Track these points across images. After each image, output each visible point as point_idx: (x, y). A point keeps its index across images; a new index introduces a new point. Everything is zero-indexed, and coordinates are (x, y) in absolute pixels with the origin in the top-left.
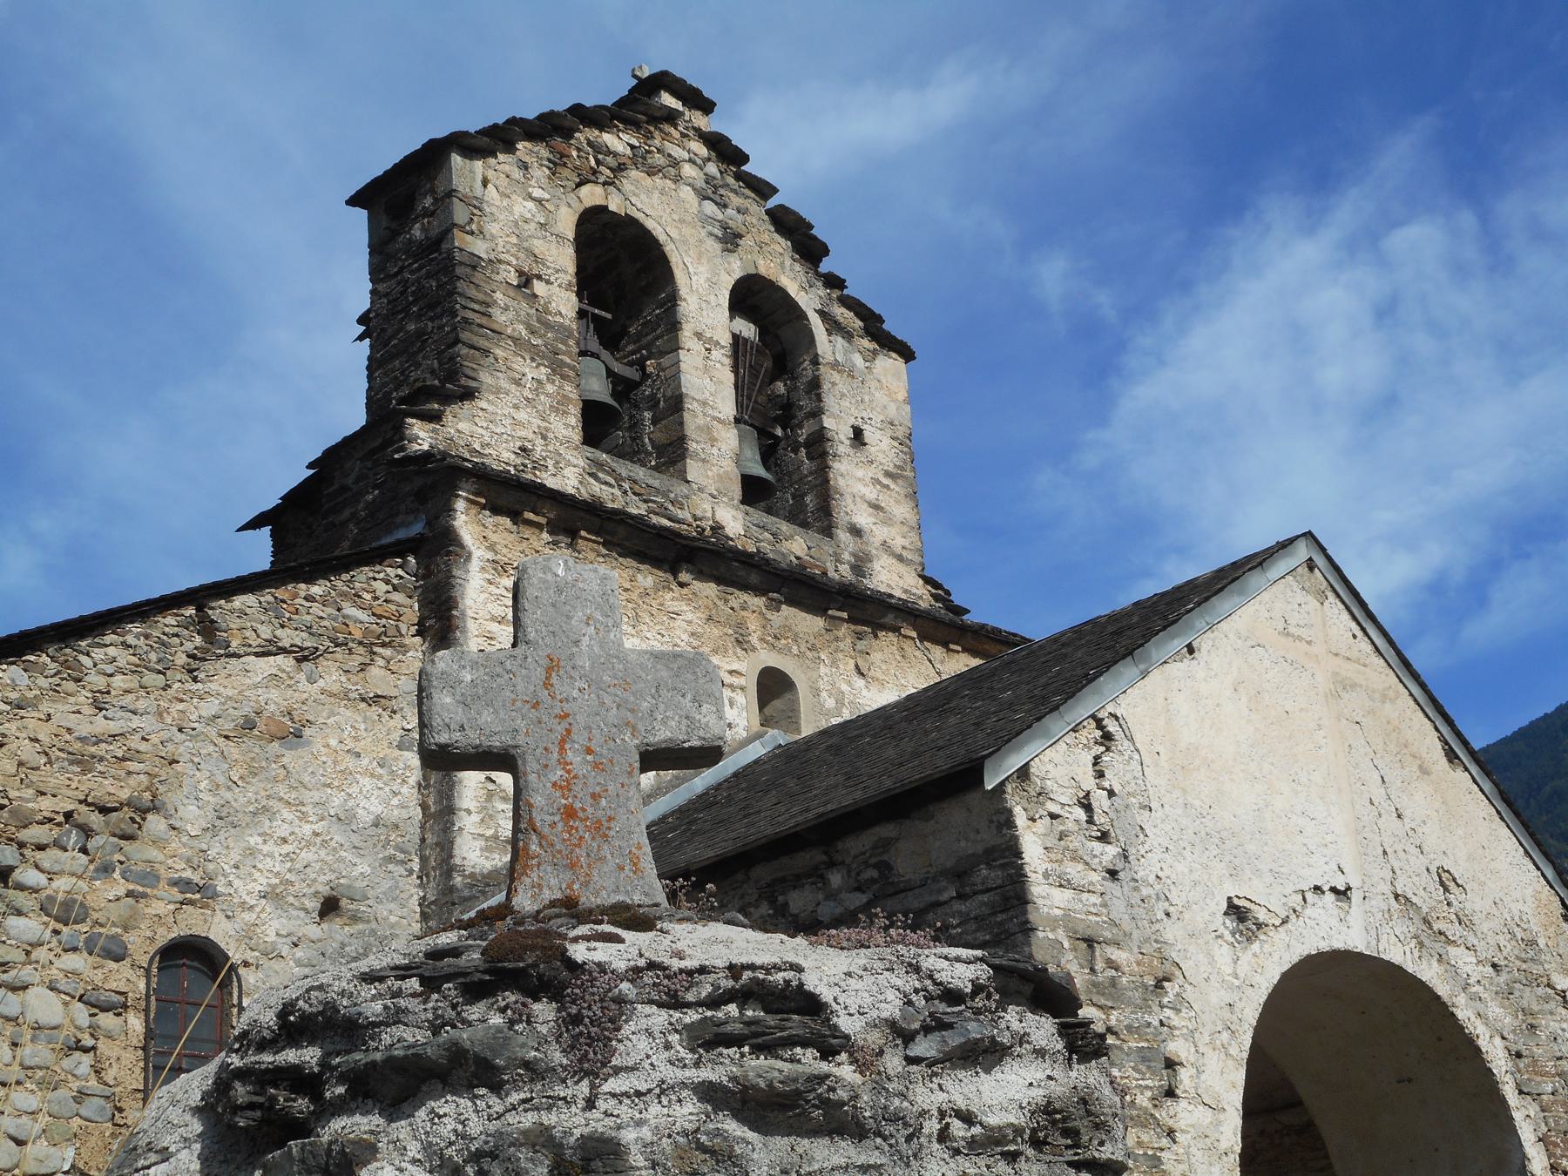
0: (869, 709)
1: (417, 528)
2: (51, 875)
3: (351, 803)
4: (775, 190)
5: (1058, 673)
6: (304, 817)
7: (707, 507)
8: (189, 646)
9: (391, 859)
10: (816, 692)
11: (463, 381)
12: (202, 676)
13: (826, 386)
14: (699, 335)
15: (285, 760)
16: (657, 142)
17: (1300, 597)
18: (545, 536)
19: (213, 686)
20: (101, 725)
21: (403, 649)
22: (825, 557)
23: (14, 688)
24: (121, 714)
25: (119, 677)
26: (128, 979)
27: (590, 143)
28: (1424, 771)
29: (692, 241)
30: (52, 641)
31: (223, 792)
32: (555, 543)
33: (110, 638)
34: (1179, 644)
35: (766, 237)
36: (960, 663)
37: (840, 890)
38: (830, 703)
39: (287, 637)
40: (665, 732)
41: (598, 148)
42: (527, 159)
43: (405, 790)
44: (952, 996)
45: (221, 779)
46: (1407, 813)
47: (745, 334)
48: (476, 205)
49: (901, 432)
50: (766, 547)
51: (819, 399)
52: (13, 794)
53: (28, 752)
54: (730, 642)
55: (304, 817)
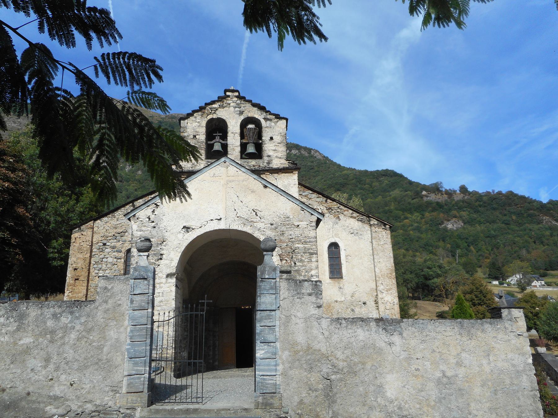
20: (118, 222)
26: (122, 255)
53: (107, 228)
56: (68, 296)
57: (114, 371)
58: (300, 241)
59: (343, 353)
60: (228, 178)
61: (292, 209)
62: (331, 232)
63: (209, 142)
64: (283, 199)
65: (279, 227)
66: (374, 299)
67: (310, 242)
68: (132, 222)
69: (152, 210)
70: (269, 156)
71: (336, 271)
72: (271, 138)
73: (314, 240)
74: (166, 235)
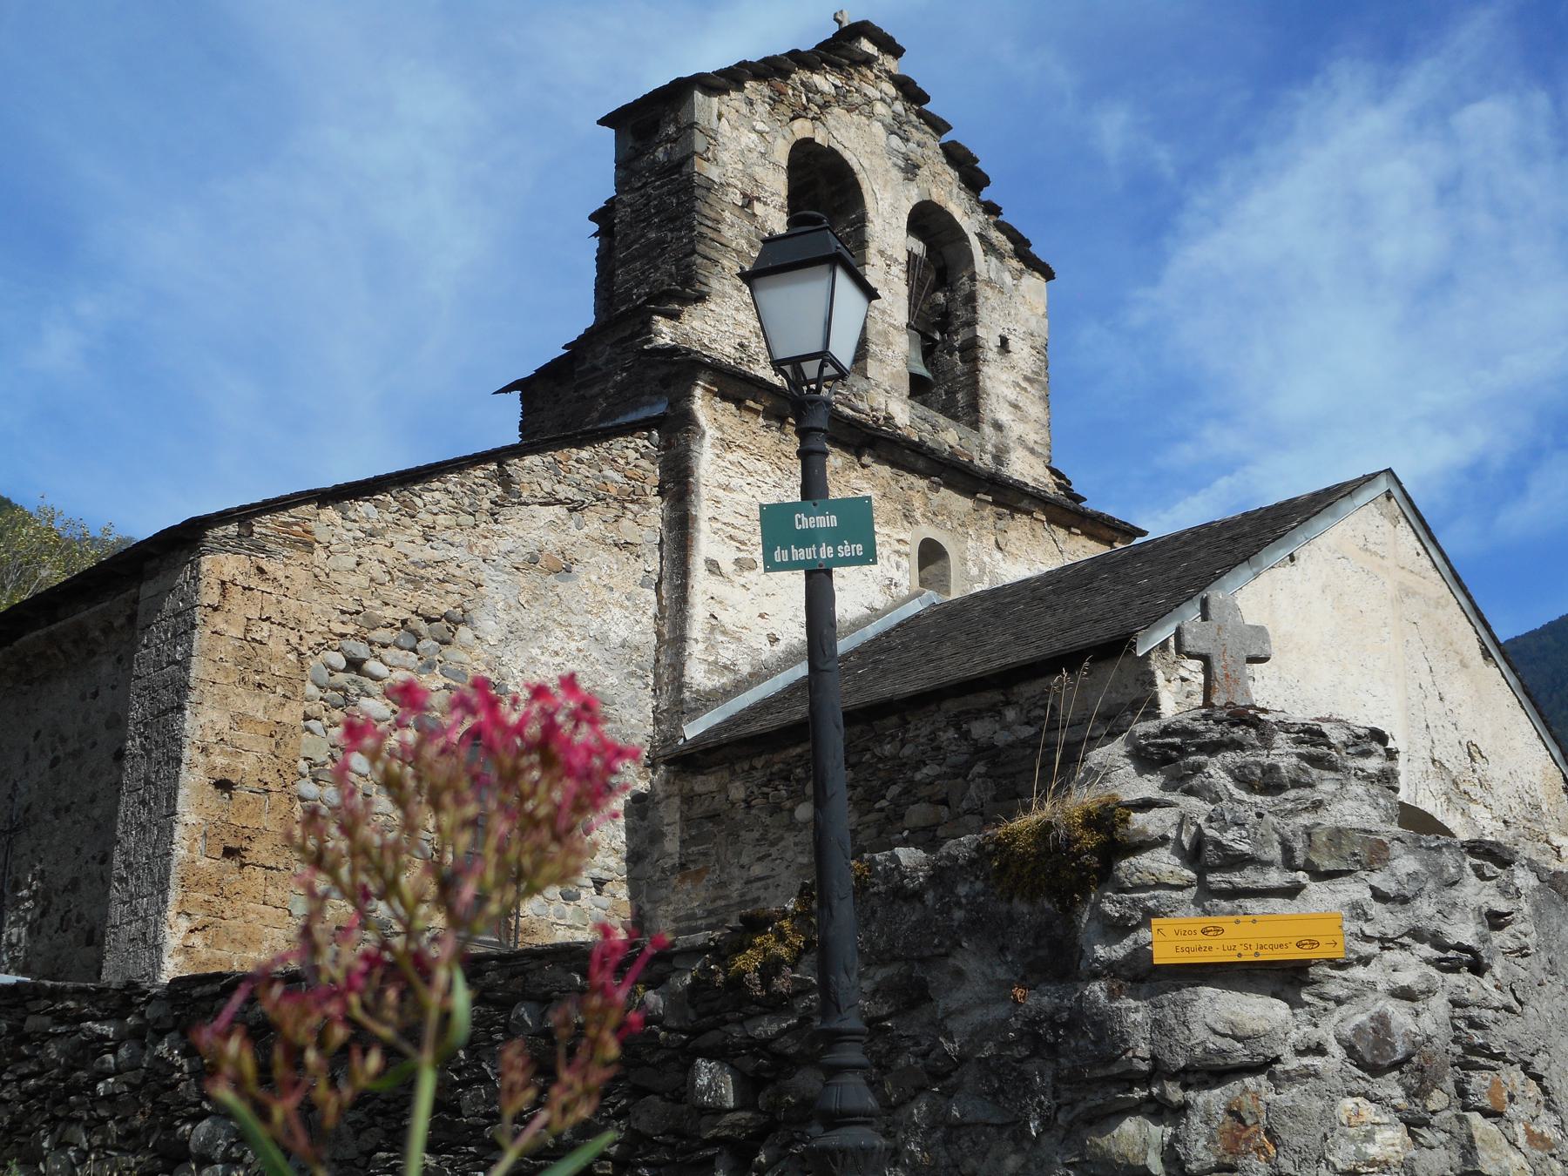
0: (1007, 582)
1: (659, 409)
2: (392, 668)
3: (605, 627)
4: (949, 128)
5: (1187, 569)
6: (570, 635)
7: (882, 400)
8: (492, 494)
9: (632, 674)
10: (964, 561)
11: (697, 286)
12: (501, 519)
13: (980, 300)
14: (882, 253)
15: (559, 590)
16: (856, 83)
17: (1379, 520)
18: (761, 420)
19: (509, 527)
20: (428, 554)
21: (647, 505)
22: (972, 447)
23: (368, 519)
24: (443, 545)
25: (442, 516)
27: (803, 83)
28: (1464, 665)
29: (880, 170)
30: (394, 485)
31: (513, 612)
32: (768, 427)
33: (436, 485)
34: (1283, 554)
35: (939, 168)
36: (1082, 549)
37: (1013, 723)
38: (974, 571)
39: (563, 491)
40: (1253, 653)
41: (809, 88)
42: (753, 96)
43: (644, 620)
44: (1358, 737)
45: (513, 602)
46: (1447, 697)
47: (916, 251)
48: (712, 136)
49: (1039, 342)
50: (926, 436)
51: (974, 311)
52: (366, 603)
53: (377, 571)
54: (899, 515)
55: (570, 635)
56: (187, 949)
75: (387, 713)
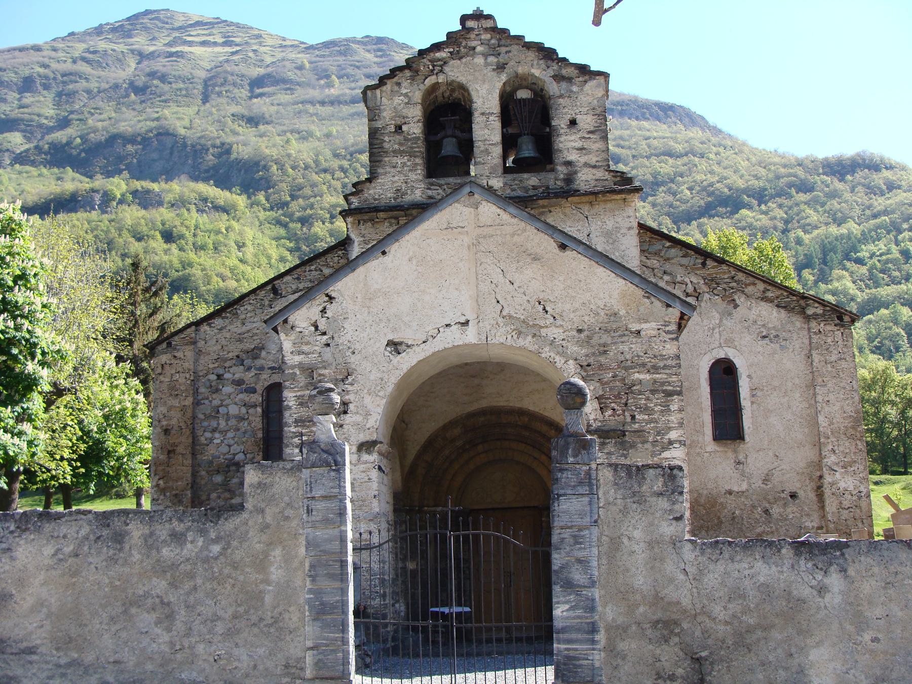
20: (244, 329)
26: (257, 398)
53: (224, 342)
57: (288, 638)
58: (644, 365)
59: (725, 608)
60: (479, 231)
61: (623, 295)
62: (717, 336)
63: (432, 138)
64: (603, 273)
65: (596, 337)
66: (813, 485)
67: (665, 367)
68: (282, 336)
69: (321, 308)
70: (569, 163)
71: (728, 424)
72: (573, 123)
73: (674, 363)
74: (352, 360)
75: (233, 390)
